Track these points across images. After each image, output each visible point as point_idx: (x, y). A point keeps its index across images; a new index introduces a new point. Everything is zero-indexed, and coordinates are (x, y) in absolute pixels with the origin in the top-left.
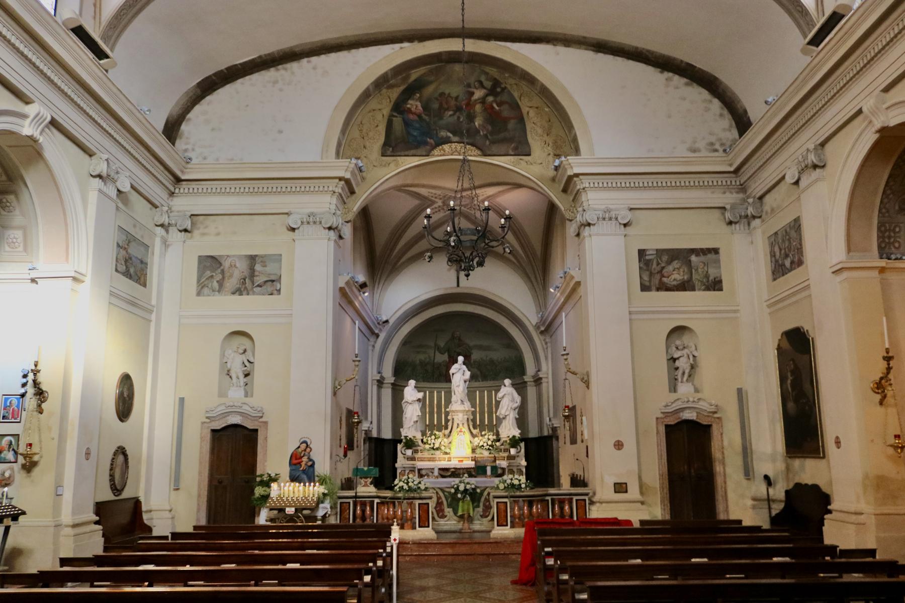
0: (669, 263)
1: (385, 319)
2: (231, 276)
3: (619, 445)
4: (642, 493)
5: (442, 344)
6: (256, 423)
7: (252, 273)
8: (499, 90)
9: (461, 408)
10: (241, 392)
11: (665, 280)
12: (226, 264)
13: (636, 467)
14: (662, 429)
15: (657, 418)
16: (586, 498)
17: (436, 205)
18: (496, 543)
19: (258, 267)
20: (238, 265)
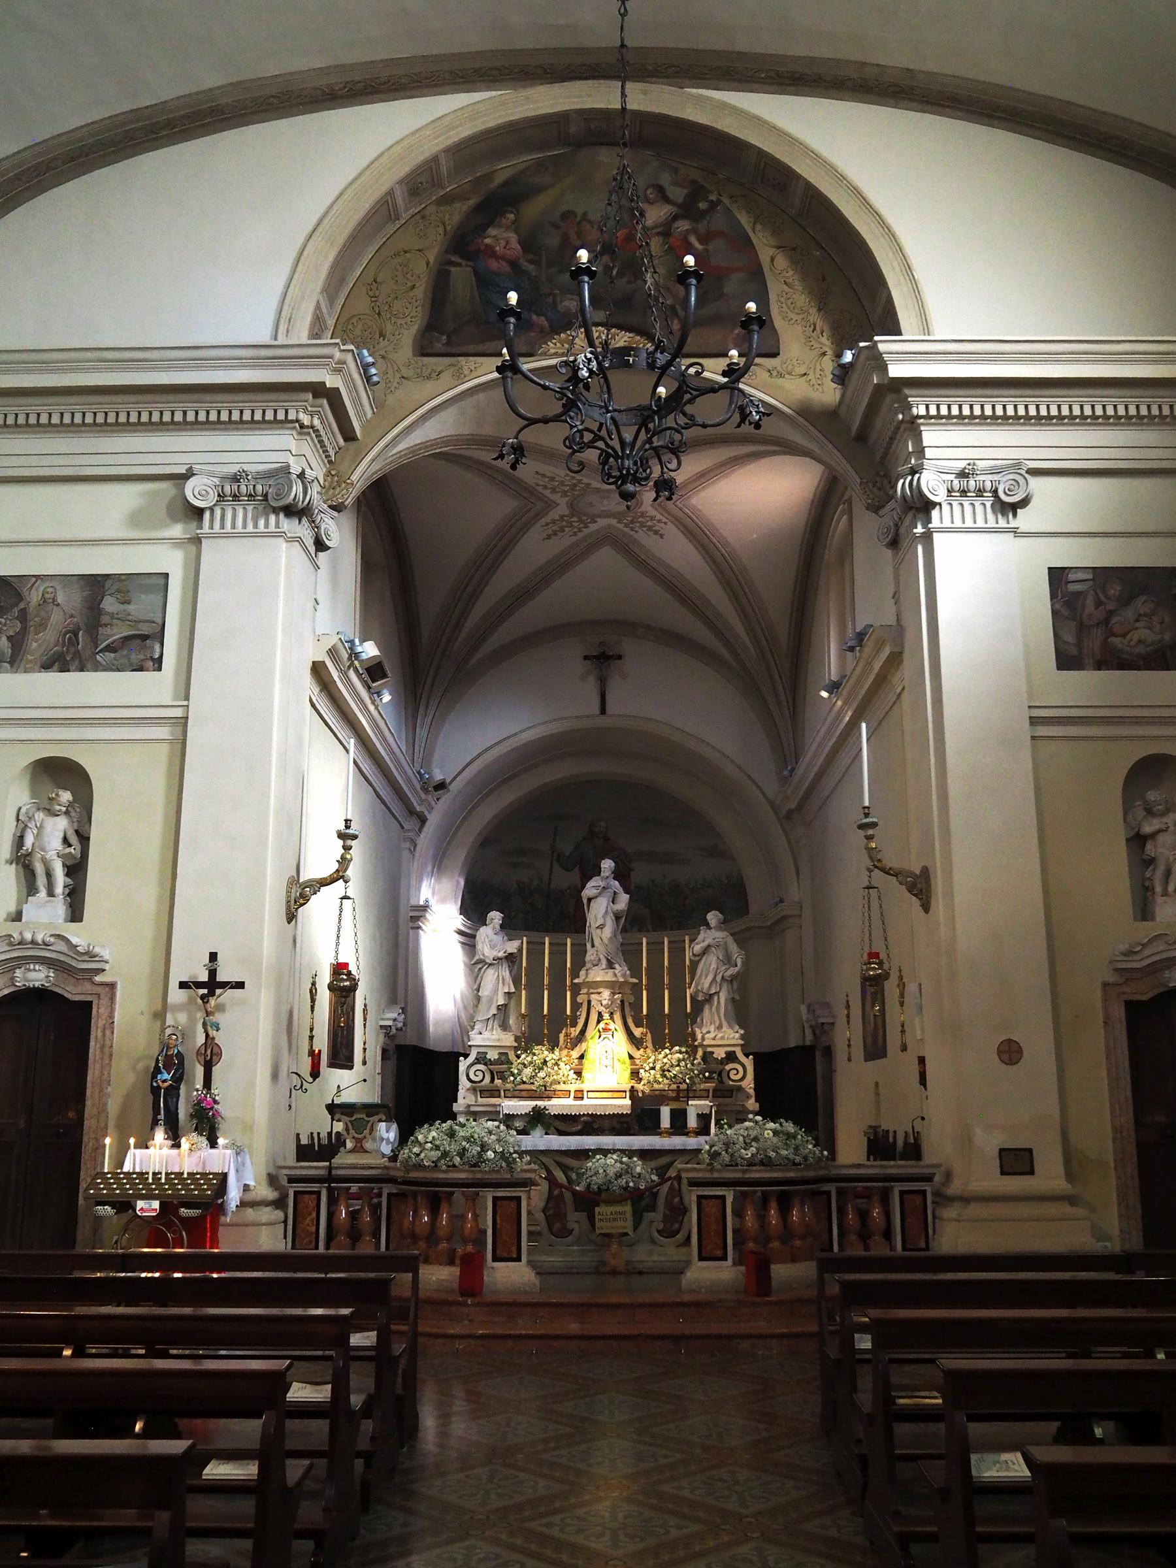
0: (1127, 600)
1: (438, 776)
2: (42, 626)
3: (1010, 1052)
4: (1069, 1176)
5: (567, 849)
6: (88, 986)
7: (94, 616)
8: (703, 205)
9: (608, 976)
10: (59, 908)
11: (1116, 640)
12: (34, 597)
13: (1056, 1114)
14: (1119, 1012)
15: (1105, 985)
16: (928, 1188)
17: (554, 514)
18: (697, 1304)
19: (109, 604)
20: (60, 599)
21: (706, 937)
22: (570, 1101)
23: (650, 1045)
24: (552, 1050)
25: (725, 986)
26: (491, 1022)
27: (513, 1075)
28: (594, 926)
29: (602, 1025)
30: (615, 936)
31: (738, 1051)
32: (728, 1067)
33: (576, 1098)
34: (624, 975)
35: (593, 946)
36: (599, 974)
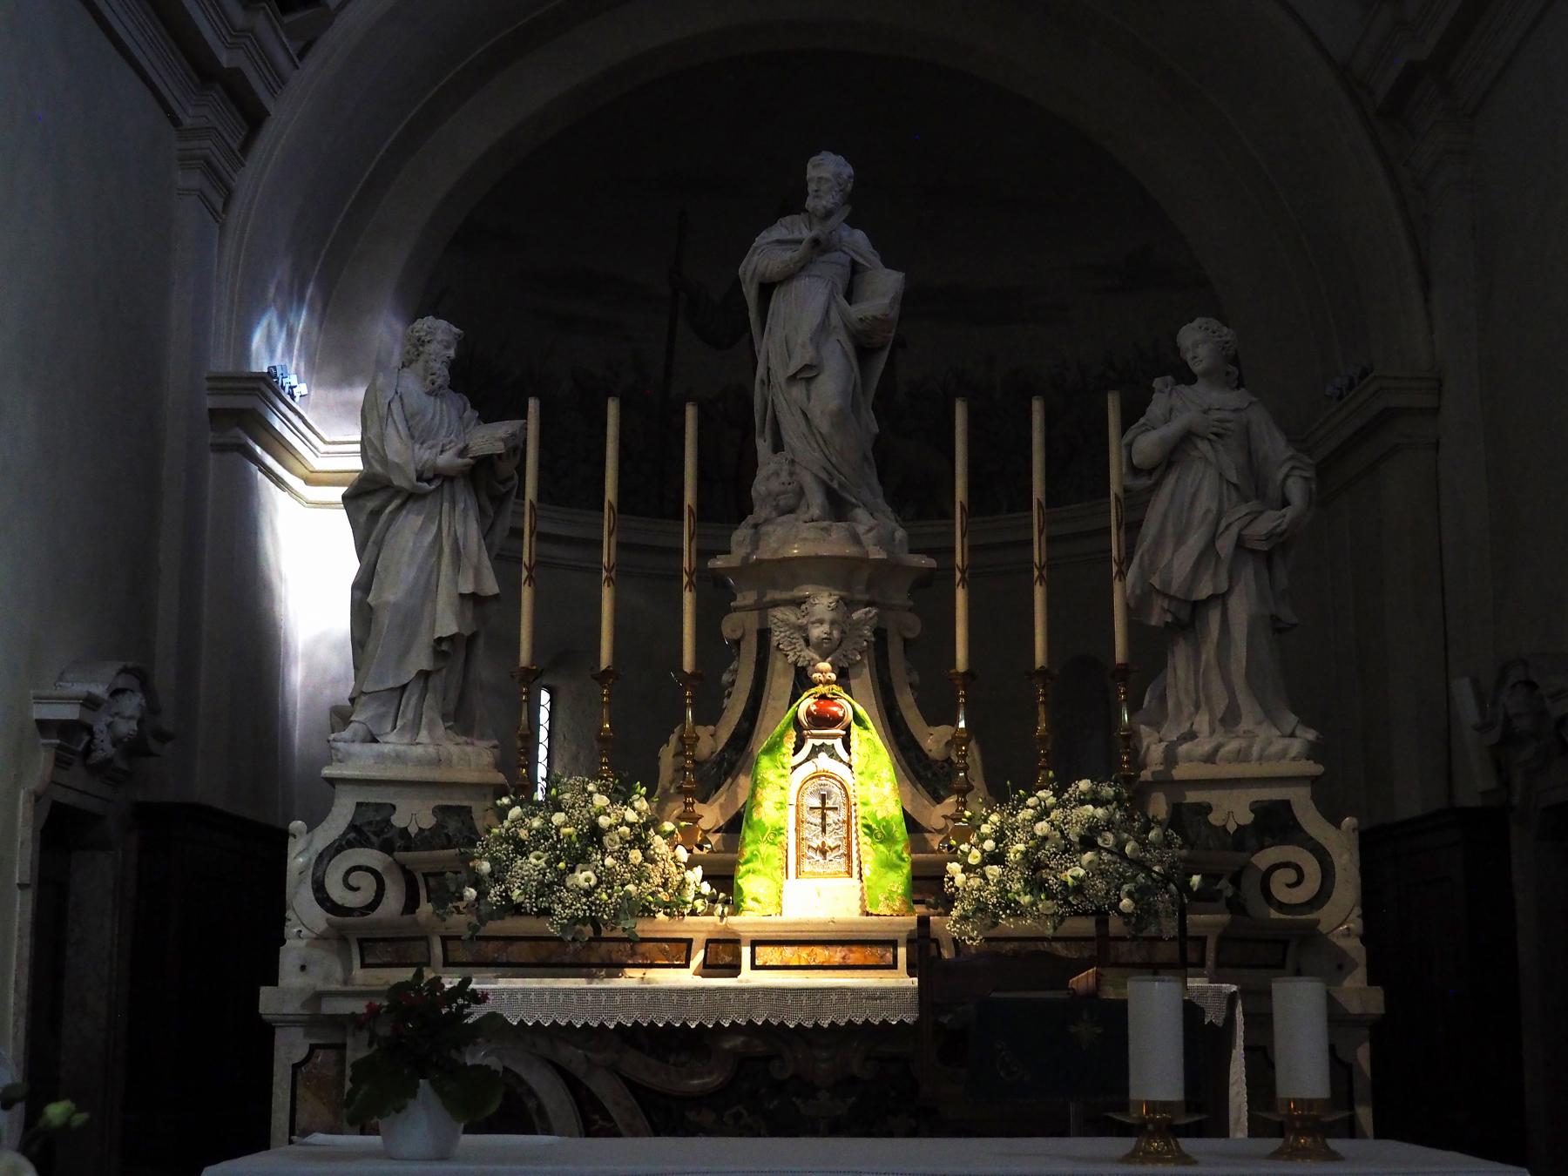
9: (834, 543)
21: (1174, 409)
22: (684, 978)
23: (978, 783)
24: (621, 796)
25: (1248, 573)
26: (410, 699)
27: (477, 881)
28: (780, 376)
29: (807, 703)
30: (855, 407)
31: (1301, 799)
32: (1266, 858)
33: (708, 968)
34: (885, 541)
35: (778, 446)
36: (799, 539)
